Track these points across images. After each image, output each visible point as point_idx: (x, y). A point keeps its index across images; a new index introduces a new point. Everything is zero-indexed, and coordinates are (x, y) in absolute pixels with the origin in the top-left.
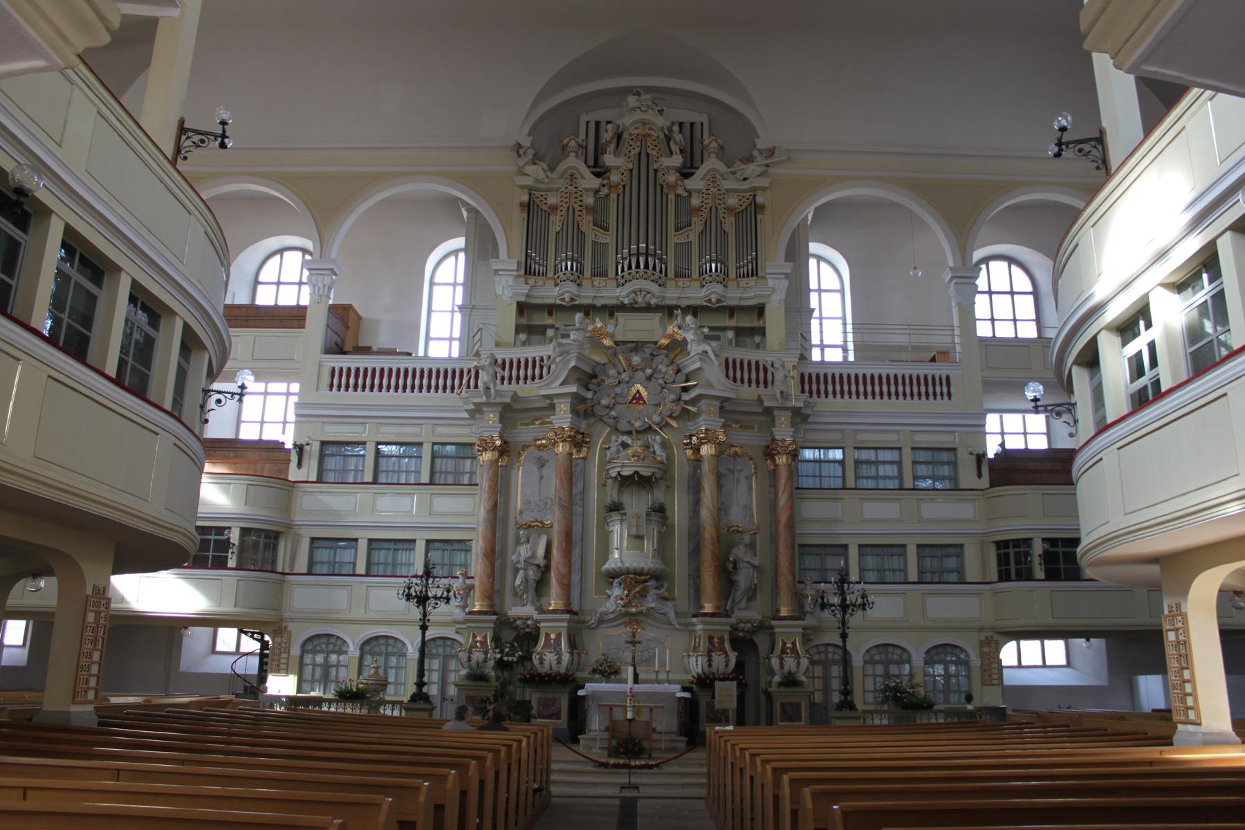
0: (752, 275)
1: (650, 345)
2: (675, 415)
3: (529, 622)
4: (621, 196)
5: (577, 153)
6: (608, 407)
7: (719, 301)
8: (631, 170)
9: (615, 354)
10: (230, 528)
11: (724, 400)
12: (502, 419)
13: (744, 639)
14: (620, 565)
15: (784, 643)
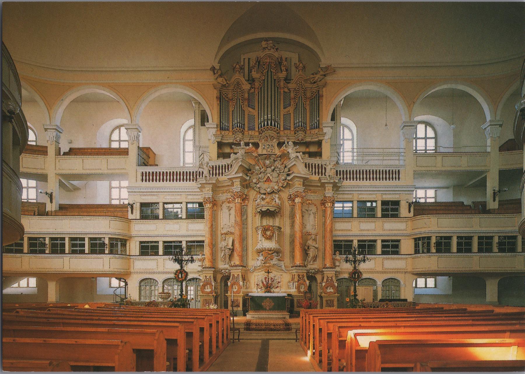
0: (317, 128)
1: (273, 156)
2: (284, 186)
3: (227, 271)
4: (260, 93)
5: (239, 72)
6: (256, 183)
7: (302, 140)
8: (264, 80)
9: (258, 160)
10: (104, 238)
11: (305, 179)
12: (213, 190)
13: (312, 276)
14: (262, 247)
15: (328, 277)
